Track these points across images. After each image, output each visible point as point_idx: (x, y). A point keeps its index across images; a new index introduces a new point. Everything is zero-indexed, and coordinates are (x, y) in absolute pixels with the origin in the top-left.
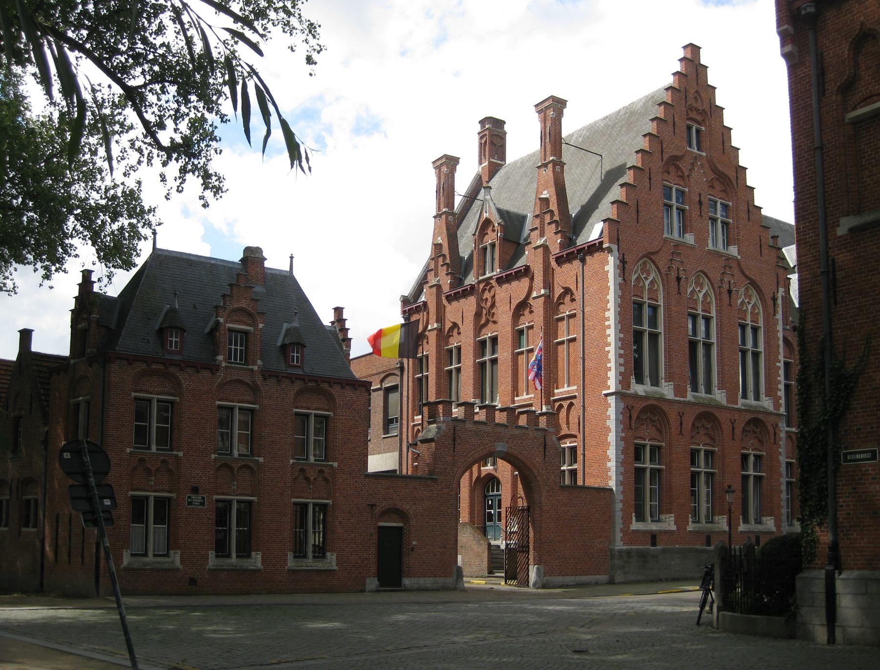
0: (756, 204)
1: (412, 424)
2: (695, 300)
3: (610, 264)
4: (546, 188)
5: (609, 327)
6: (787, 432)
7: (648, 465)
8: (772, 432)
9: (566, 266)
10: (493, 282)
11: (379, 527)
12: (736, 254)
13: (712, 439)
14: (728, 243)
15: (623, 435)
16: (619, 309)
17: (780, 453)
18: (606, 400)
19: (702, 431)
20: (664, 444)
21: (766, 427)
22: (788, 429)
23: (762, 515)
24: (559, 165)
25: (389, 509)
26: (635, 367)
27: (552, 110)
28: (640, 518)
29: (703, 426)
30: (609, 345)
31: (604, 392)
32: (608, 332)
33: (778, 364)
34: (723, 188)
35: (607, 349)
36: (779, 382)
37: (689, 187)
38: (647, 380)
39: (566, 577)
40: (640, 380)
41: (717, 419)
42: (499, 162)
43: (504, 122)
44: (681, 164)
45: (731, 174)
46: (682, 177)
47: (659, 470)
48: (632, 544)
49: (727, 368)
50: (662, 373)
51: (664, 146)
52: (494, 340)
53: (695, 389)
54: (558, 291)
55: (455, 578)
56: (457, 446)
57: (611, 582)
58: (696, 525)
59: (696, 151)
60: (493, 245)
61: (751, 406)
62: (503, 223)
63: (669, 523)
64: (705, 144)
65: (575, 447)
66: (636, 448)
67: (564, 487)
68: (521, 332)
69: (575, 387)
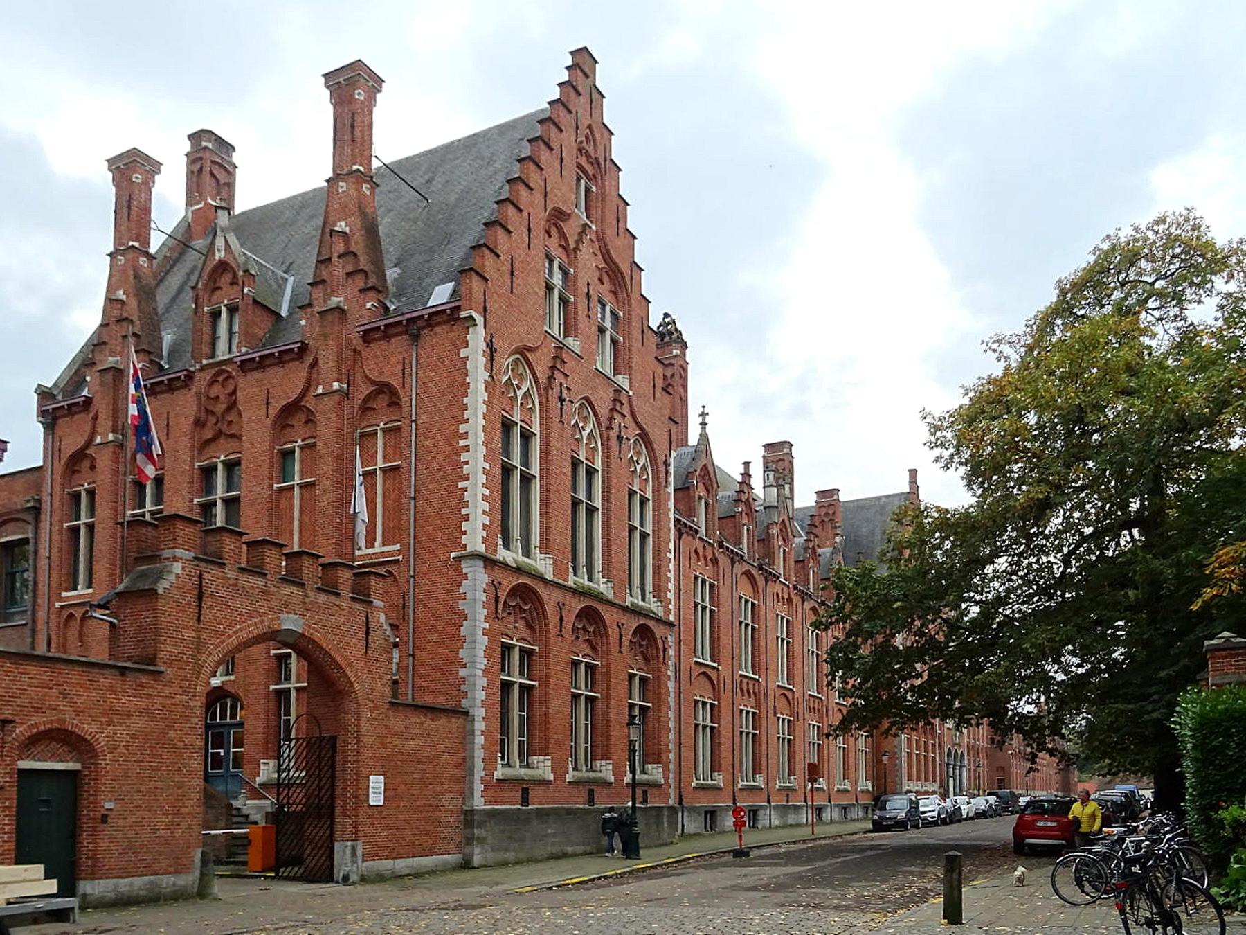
1: (57, 605)
8: (661, 647)
9: (378, 348)
11: (22, 772)
13: (594, 649)
29: (584, 629)
41: (602, 620)
43: (233, 148)
45: (625, 268)
48: (496, 803)
49: (614, 547)
50: (536, 539)
57: (466, 865)
58: (576, 773)
59: (584, 216)
61: (637, 606)
63: (543, 767)
69: (398, 547)
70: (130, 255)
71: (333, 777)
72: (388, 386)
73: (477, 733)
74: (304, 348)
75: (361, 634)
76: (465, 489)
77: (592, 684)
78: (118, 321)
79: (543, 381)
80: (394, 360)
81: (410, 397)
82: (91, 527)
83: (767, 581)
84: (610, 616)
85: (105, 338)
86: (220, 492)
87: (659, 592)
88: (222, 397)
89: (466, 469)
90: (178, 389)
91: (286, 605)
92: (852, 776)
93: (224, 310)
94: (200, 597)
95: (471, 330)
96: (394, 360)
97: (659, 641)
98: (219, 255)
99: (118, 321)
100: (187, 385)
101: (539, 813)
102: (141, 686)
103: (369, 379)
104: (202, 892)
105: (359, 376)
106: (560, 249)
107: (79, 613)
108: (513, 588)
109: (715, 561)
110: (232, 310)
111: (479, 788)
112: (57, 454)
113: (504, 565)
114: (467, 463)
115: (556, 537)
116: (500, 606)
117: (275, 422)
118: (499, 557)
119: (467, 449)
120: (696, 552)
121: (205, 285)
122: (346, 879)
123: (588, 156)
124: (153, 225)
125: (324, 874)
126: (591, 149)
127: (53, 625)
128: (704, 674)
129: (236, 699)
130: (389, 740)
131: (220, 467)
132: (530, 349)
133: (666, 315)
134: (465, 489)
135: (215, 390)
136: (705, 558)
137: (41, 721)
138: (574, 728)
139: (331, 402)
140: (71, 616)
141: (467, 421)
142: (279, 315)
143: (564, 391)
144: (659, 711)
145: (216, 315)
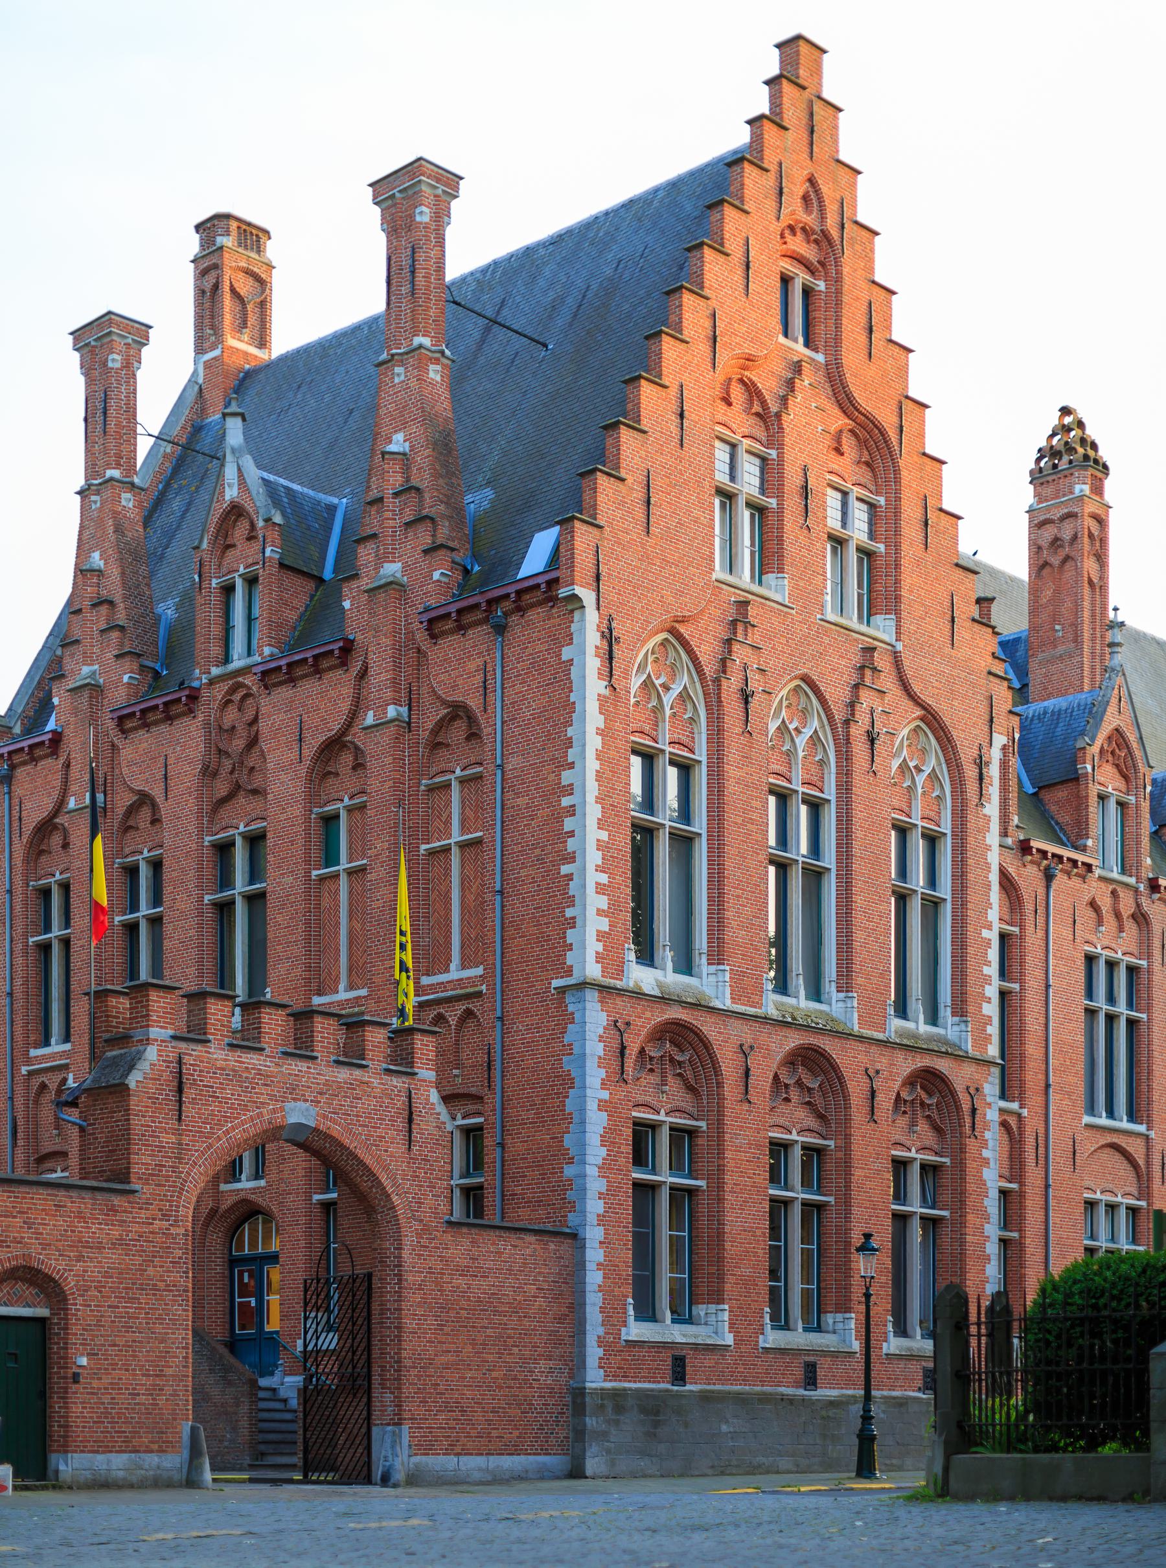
1: (24, 1070)
4: (403, 426)
6: (1002, 1111)
7: (666, 1177)
9: (451, 645)
13: (821, 1117)
17: (986, 1162)
18: (561, 1003)
19: (794, 1094)
20: (703, 1124)
21: (953, 1093)
22: (1003, 1104)
25: (15, 1269)
27: (412, 200)
28: (646, 1312)
29: (799, 1083)
31: (556, 983)
33: (985, 933)
34: (866, 457)
36: (987, 980)
38: (666, 956)
39: (463, 1459)
40: (647, 956)
43: (266, 232)
45: (887, 419)
47: (691, 1192)
50: (701, 940)
53: (782, 986)
55: (186, 1454)
59: (799, 347)
61: (915, 1036)
65: (479, 1128)
66: (635, 1133)
69: (479, 971)
70: (108, 493)
72: (465, 707)
74: (348, 648)
75: (401, 1124)
76: (570, 877)
78: (94, 606)
80: (472, 666)
81: (493, 725)
82: (66, 942)
85: (77, 633)
86: (240, 884)
88: (240, 727)
89: (571, 845)
90: (178, 716)
93: (239, 583)
95: (577, 615)
96: (472, 666)
98: (231, 493)
99: (94, 606)
100: (191, 711)
101: (706, 1398)
103: (439, 697)
104: (191, 1482)
105: (424, 690)
106: (753, 420)
108: (660, 1024)
110: (252, 581)
111: (594, 1353)
112: (16, 824)
113: (637, 995)
114: (571, 834)
116: (630, 1062)
117: (311, 770)
119: (571, 811)
120: (1093, 904)
121: (214, 542)
122: (385, 1480)
124: (139, 430)
125: (361, 1472)
127: (19, 1101)
129: (268, 1216)
130: (446, 1278)
131: (239, 842)
132: (683, 620)
134: (570, 877)
135: (231, 716)
136: (1118, 915)
139: (384, 738)
140: (43, 1086)
141: (571, 766)
142: (320, 580)
144: (963, 1224)
145: (228, 590)
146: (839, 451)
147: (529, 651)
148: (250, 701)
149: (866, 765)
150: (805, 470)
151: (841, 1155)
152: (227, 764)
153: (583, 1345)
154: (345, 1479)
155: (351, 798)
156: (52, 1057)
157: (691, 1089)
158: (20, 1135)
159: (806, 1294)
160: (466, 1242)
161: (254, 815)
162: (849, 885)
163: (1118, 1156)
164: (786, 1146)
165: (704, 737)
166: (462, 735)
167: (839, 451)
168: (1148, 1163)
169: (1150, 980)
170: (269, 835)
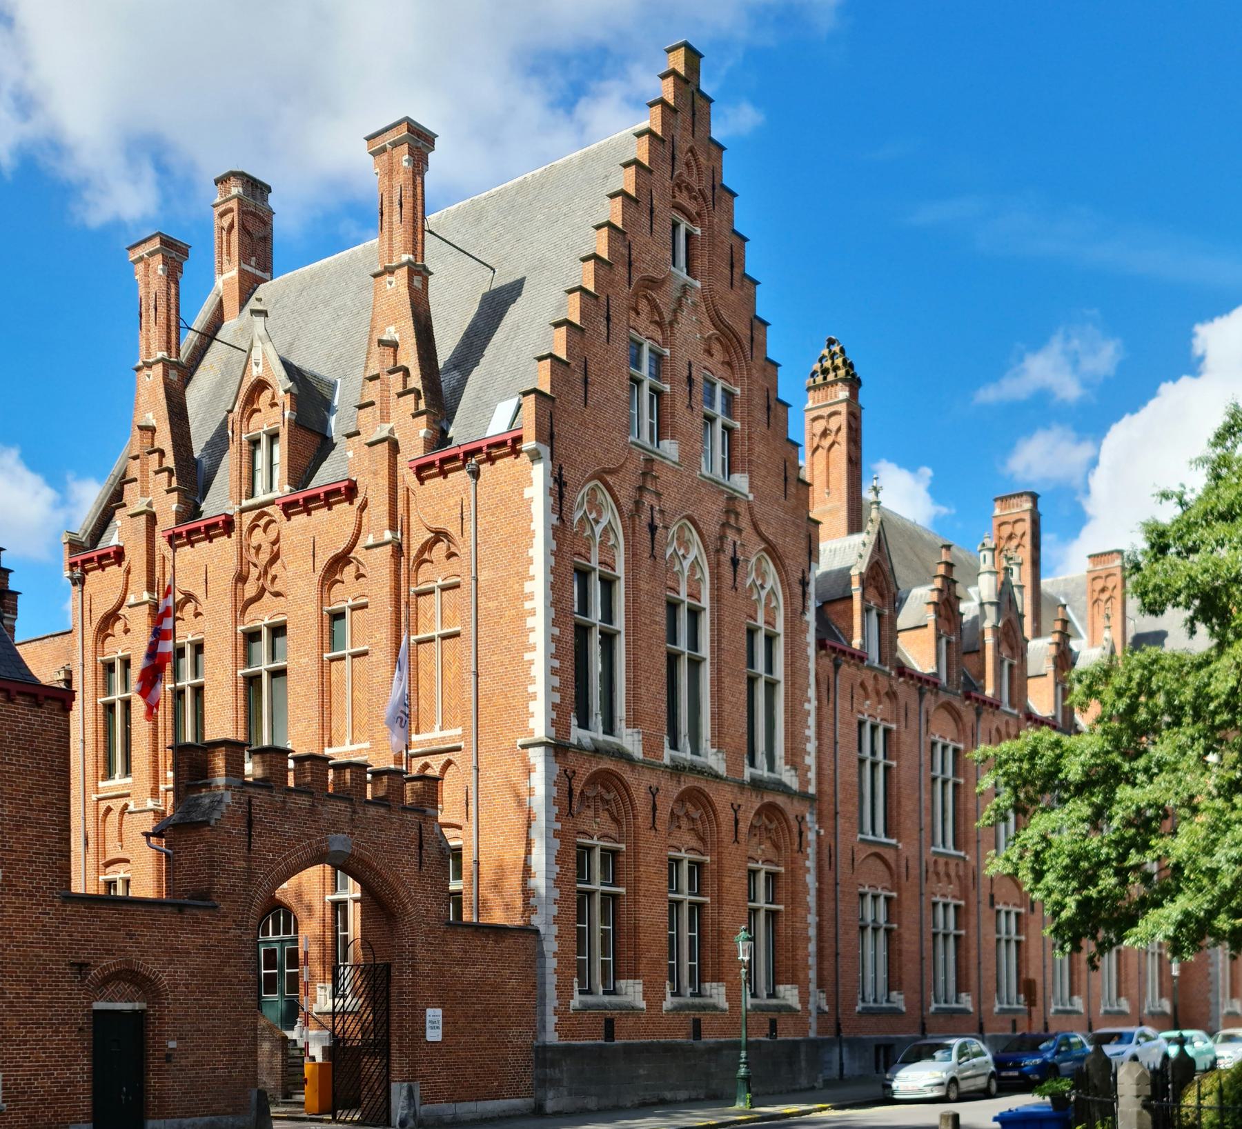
0: (781, 396)
1: (94, 797)
2: (676, 574)
3: (535, 481)
4: (394, 321)
5: (533, 613)
8: (795, 830)
10: (275, 511)
12: (746, 490)
13: (702, 839)
14: (731, 467)
15: (558, 826)
16: (551, 578)
17: (808, 870)
19: (684, 823)
20: (623, 846)
23: (776, 982)
24: (419, 273)
26: (576, 693)
29: (687, 815)
30: (534, 648)
32: (530, 622)
35: (527, 656)
37: (672, 347)
39: (459, 1105)
40: (584, 724)
42: (259, 273)
44: (660, 298)
45: (743, 330)
46: (659, 324)
49: (727, 707)
50: (621, 710)
51: (634, 253)
52: (278, 630)
53: (674, 746)
54: (419, 537)
56: (255, 839)
57: (538, 1111)
58: (677, 1000)
59: (684, 274)
60: (273, 437)
62: (295, 391)
64: (700, 264)
67: (449, 924)
68: (338, 616)
69: (459, 731)
71: (388, 1009)
72: (446, 535)
73: (549, 955)
75: (414, 849)
77: (697, 884)
79: (628, 505)
83: (978, 714)
84: (722, 798)
87: (794, 758)
91: (334, 824)
92: (1134, 992)
94: (250, 825)
96: (452, 502)
97: (794, 823)
101: (629, 1050)
102: (197, 922)
106: (652, 327)
107: (117, 805)
108: (595, 773)
109: (892, 695)
111: (552, 1020)
112: (87, 614)
113: (580, 748)
115: (646, 706)
118: (573, 740)
123: (689, 189)
126: (693, 181)
128: (878, 856)
132: (611, 472)
133: (831, 342)
136: (878, 693)
137: (110, 963)
138: (673, 944)
140: (109, 810)
143: (657, 516)
144: (794, 914)
146: (709, 352)
147: (497, 491)
148: (272, 525)
149: (731, 583)
150: (690, 365)
151: (715, 867)
152: (254, 572)
153: (543, 1014)
154: (367, 1121)
155: (354, 599)
156: (115, 788)
157: (616, 820)
158: (91, 845)
159: (691, 968)
160: (461, 940)
161: (275, 611)
162: (719, 670)
163: (878, 862)
164: (678, 861)
165: (622, 559)
166: (444, 553)
167: (709, 352)
168: (898, 866)
169: (898, 738)
170: (289, 626)
